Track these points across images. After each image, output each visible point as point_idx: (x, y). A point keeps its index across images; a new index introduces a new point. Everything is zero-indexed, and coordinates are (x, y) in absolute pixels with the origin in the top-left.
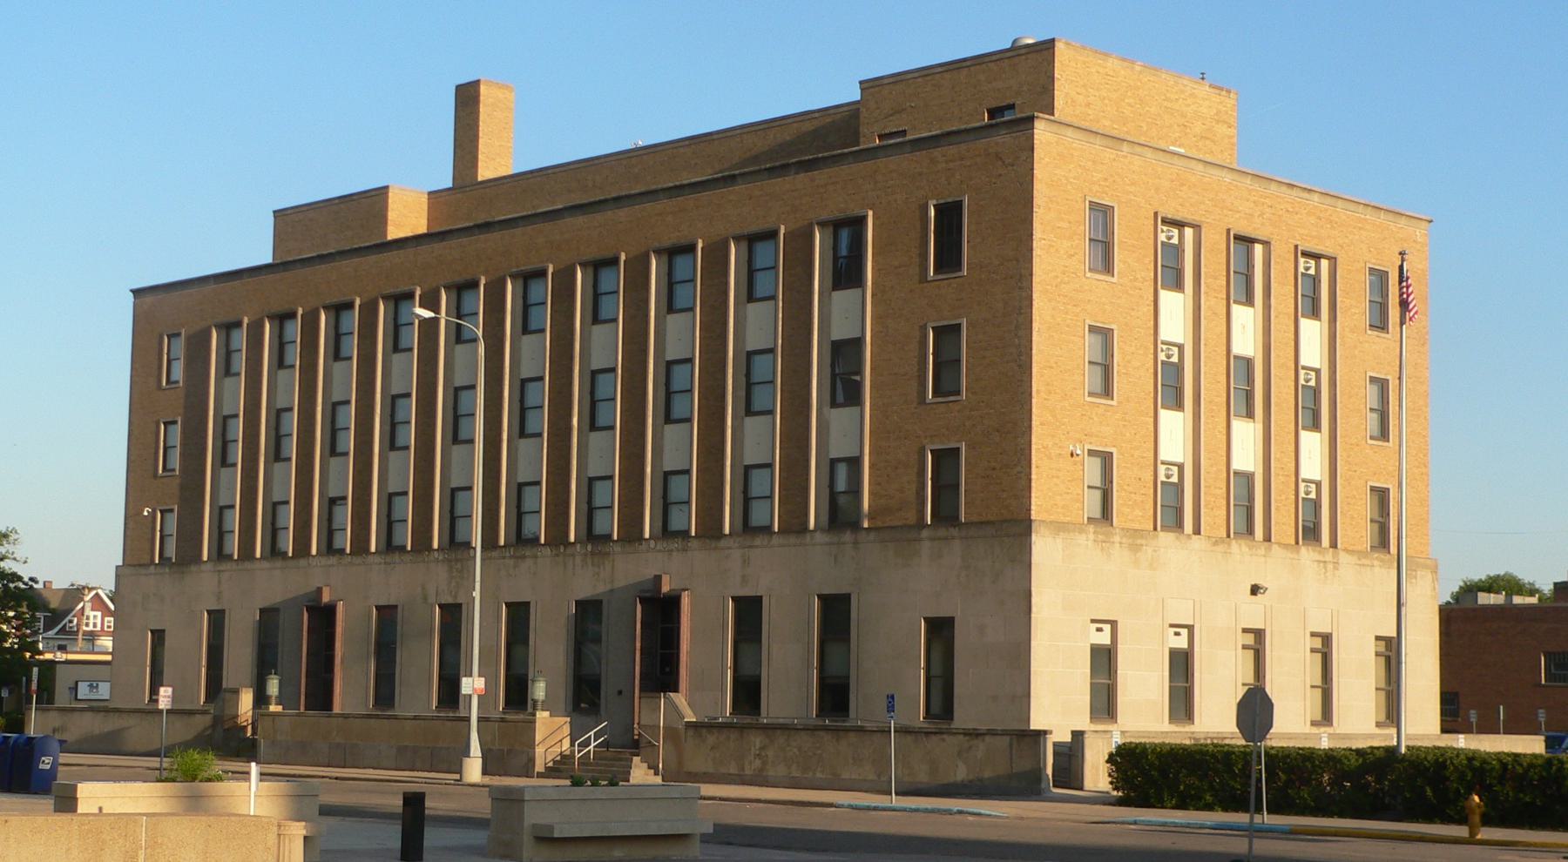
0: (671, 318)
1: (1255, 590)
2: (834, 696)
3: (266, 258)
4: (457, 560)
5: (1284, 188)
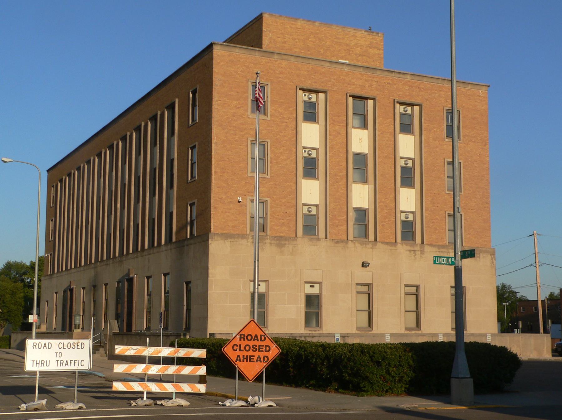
1: (364, 265)
5: (387, 73)
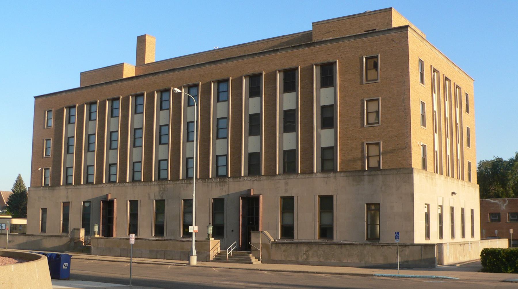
0: (136, 116)
1: (453, 193)
2: (326, 232)
3: (78, 86)
4: (162, 185)
